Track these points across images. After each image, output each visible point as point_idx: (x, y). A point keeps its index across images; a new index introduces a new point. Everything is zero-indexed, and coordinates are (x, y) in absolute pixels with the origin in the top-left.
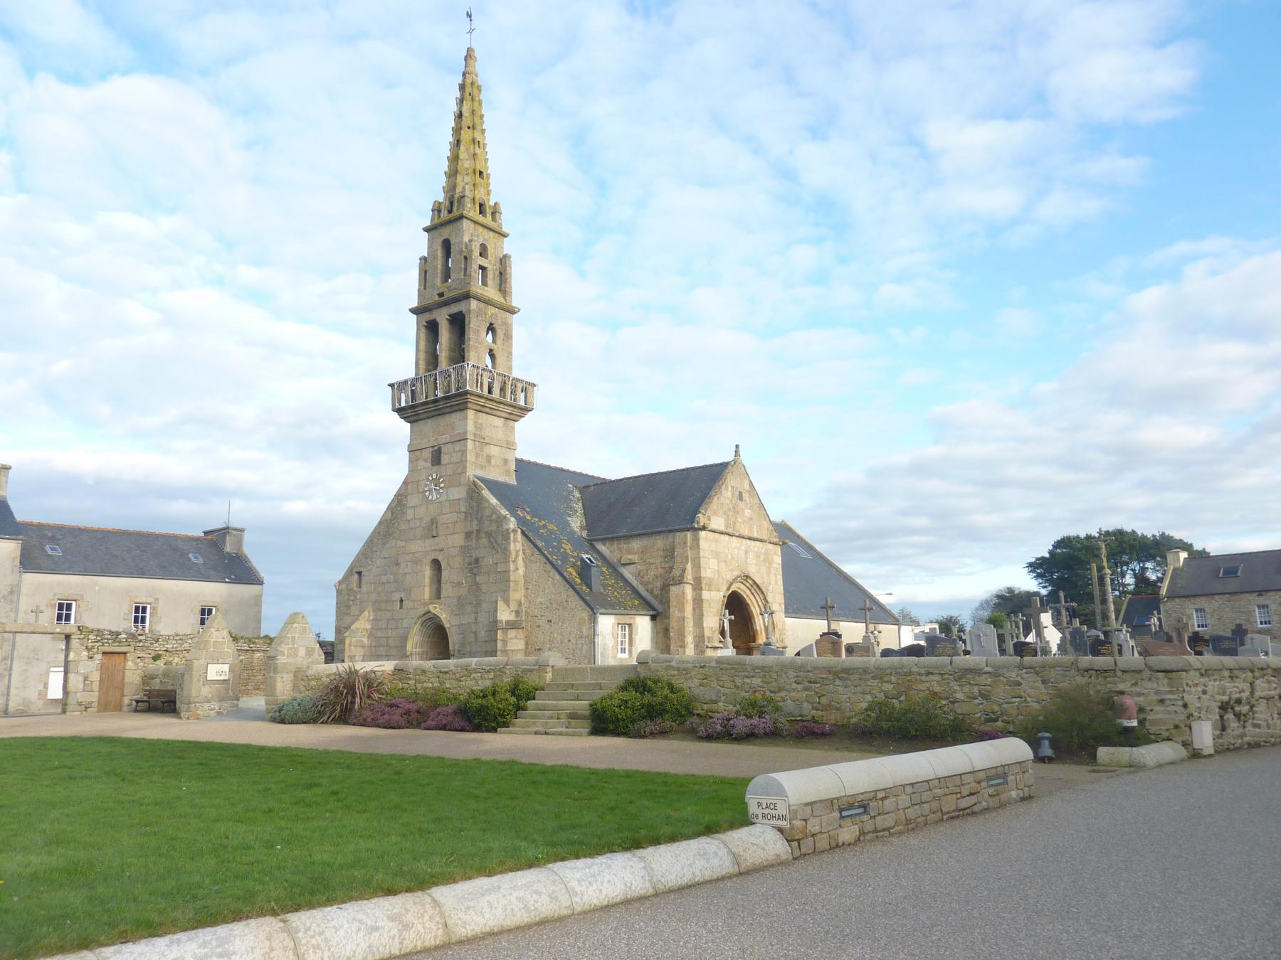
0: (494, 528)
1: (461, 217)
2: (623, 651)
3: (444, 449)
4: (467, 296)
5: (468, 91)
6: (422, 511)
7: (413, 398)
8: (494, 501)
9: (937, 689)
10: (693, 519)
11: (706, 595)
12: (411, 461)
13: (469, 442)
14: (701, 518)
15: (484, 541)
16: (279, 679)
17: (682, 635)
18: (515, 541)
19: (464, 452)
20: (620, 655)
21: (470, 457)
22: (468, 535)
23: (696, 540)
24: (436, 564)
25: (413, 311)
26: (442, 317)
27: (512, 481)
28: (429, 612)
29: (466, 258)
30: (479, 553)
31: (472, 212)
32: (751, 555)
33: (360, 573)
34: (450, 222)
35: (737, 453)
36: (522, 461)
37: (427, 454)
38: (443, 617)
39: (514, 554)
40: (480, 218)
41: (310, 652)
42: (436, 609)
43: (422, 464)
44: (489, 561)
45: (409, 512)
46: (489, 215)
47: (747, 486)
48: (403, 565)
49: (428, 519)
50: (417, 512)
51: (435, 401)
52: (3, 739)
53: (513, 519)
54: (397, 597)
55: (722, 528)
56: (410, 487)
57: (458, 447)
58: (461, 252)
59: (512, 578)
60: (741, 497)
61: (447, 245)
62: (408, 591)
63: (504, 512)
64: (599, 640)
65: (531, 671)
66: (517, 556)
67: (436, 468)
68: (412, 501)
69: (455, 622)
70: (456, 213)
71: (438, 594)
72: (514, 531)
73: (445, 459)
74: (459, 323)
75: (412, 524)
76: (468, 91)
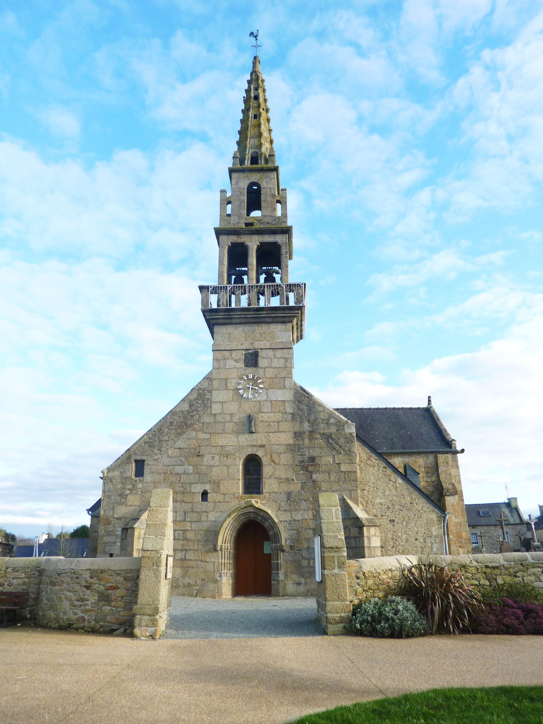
0: (333, 430)
3: (262, 354)
5: (255, 81)
6: (233, 407)
15: (321, 442)
22: (298, 435)
23: (456, 461)
30: (315, 453)
34: (262, 170)
43: (231, 363)
45: (214, 406)
49: (243, 415)
52: (542, 636)
54: (199, 489)
58: (273, 196)
62: (217, 484)
67: (250, 370)
69: (287, 517)
73: (262, 362)
75: (219, 418)
76: (255, 81)
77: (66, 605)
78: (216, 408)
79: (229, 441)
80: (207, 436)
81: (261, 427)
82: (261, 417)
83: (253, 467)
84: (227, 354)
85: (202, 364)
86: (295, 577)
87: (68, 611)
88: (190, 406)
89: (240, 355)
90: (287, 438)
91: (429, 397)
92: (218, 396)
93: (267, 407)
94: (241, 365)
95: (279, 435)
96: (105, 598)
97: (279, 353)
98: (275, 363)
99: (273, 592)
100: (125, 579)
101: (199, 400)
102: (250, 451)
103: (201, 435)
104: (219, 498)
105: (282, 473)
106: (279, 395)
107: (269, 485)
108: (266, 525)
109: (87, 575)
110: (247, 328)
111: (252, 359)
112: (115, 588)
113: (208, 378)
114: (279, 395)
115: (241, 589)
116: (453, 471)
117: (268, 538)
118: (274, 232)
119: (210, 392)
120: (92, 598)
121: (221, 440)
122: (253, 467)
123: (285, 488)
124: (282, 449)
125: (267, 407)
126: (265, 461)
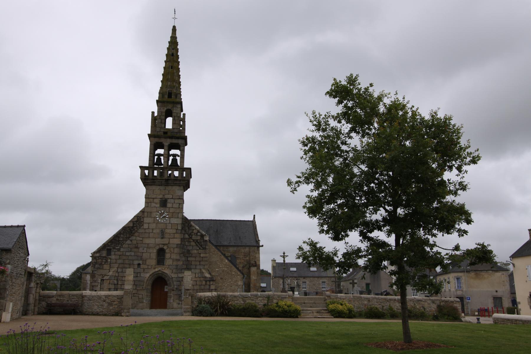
3: (169, 201)
6: (153, 226)
22: (183, 240)
23: (259, 250)
73: (169, 205)
75: (147, 231)
77: (96, 307)
78: (146, 226)
79: (151, 241)
80: (141, 239)
81: (167, 236)
82: (167, 231)
83: (161, 253)
84: (152, 200)
85: (140, 204)
86: (178, 301)
87: (96, 309)
88: (133, 224)
89: (157, 201)
90: (178, 241)
91: (254, 215)
92: (146, 220)
93: (169, 226)
94: (158, 205)
95: (174, 239)
96: (110, 304)
97: (177, 201)
98: (175, 206)
99: (168, 307)
100: (118, 298)
101: (137, 222)
102: (161, 246)
103: (138, 238)
104: (146, 267)
105: (174, 256)
106: (174, 221)
107: (168, 262)
108: (166, 279)
109: (104, 297)
110: (162, 188)
111: (164, 203)
112: (114, 301)
113: (142, 211)
114: (174, 221)
115: (168, 97)
116: (257, 256)
117: (167, 285)
118: (178, 138)
119: (143, 218)
120: (106, 305)
121: (147, 241)
122: (161, 253)
123: (175, 263)
124: (175, 246)
125: (169, 226)
126: (167, 251)
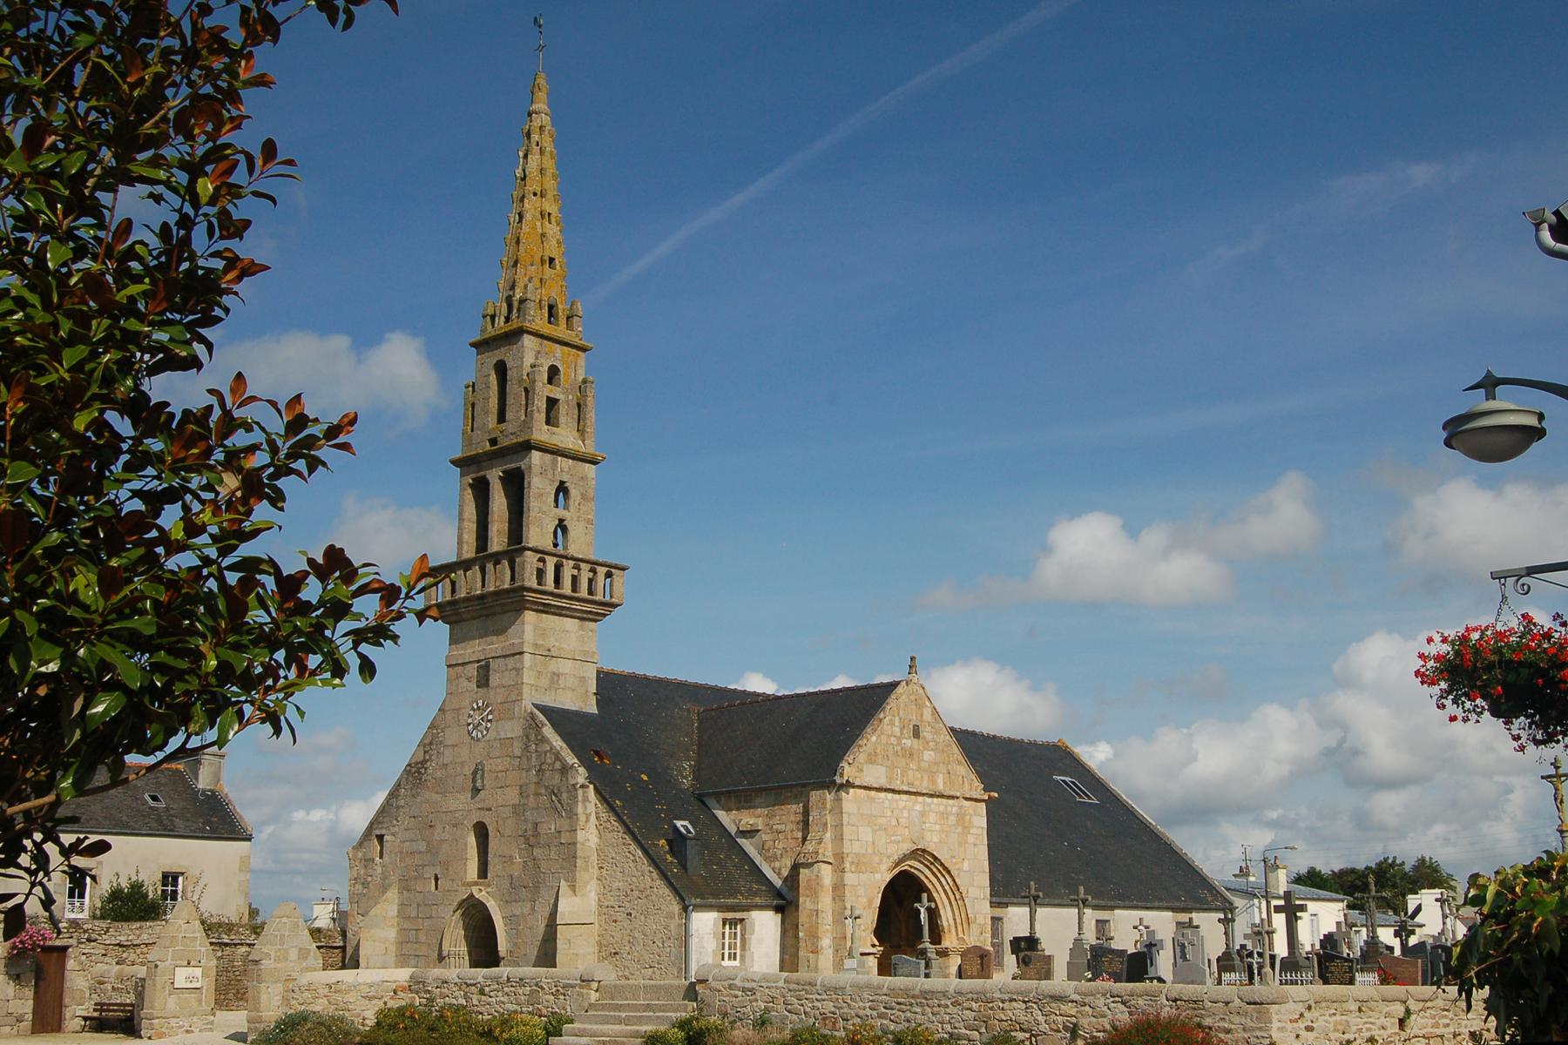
1: (520, 332)
2: (733, 957)
3: (494, 664)
4: (527, 447)
7: (453, 591)
8: (558, 742)
9: (1022, 1019)
10: (834, 770)
11: (850, 878)
12: (449, 680)
13: (527, 657)
14: (848, 771)
16: (263, 990)
17: (814, 936)
18: (586, 800)
19: (519, 671)
20: (726, 963)
21: (528, 677)
24: (482, 832)
25: (455, 463)
26: (494, 476)
27: (592, 709)
28: (472, 896)
29: (526, 390)
31: (538, 321)
32: (932, 817)
33: (380, 838)
35: (140, 995)
36: (607, 674)
37: (472, 670)
38: (492, 906)
39: (582, 818)
40: (547, 329)
41: (303, 953)
42: (481, 895)
44: (549, 827)
45: (448, 752)
46: (563, 322)
47: (927, 713)
48: (438, 829)
50: (460, 755)
51: (482, 597)
53: (582, 770)
54: (429, 872)
55: (883, 782)
56: (449, 716)
57: (511, 662)
58: (521, 381)
59: (579, 853)
60: (916, 733)
61: (501, 369)
62: (446, 865)
63: (571, 759)
64: (694, 943)
65: (573, 986)
66: (587, 820)
68: (452, 736)
70: (514, 324)
71: (483, 872)
72: (582, 786)
73: (494, 679)
74: (516, 484)
